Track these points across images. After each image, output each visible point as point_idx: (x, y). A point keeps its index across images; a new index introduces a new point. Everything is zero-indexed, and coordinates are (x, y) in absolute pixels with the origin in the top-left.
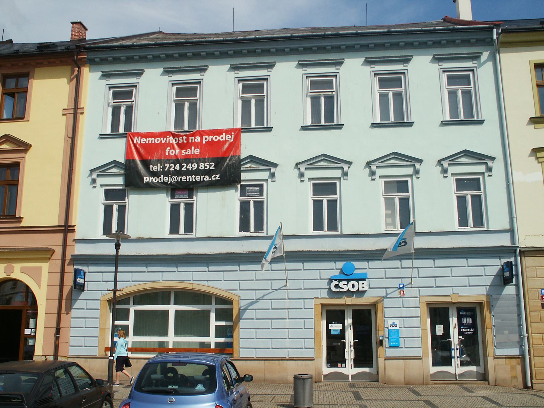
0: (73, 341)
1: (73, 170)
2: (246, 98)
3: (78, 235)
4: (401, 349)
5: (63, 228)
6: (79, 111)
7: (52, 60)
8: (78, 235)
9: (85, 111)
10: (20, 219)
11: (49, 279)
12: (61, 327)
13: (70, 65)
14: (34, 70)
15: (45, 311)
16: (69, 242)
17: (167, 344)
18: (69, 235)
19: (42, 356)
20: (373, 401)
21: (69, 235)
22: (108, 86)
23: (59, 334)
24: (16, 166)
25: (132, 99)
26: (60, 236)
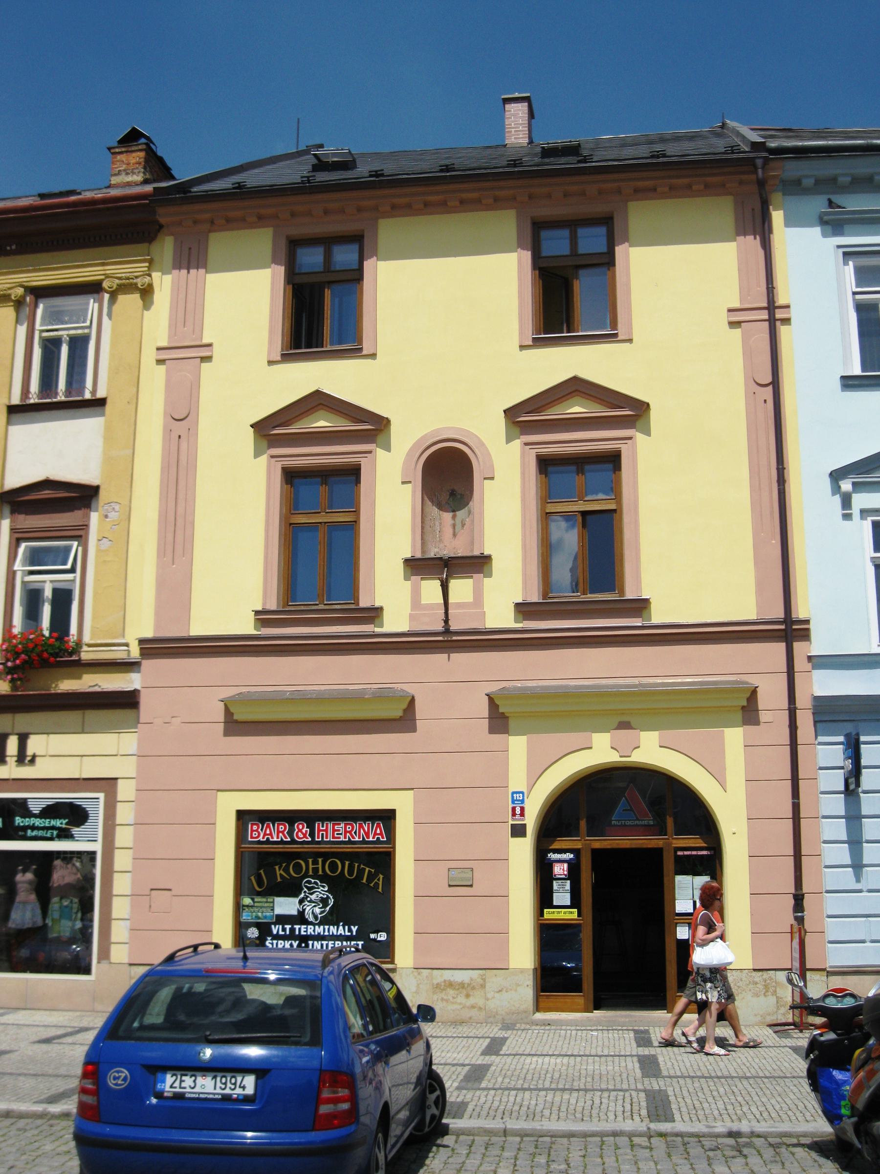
0: (834, 929)
1: (785, 471)
2: (536, 317)
3: (819, 645)
4: (203, 955)
5: (783, 627)
6: (779, 314)
7: (680, 181)
8: (819, 645)
9: (794, 314)
10: (374, 614)
11: (749, 763)
12: (804, 891)
13: (730, 194)
14: (626, 207)
15: (413, 857)
16: (800, 664)
17: (239, 944)
18: (797, 646)
19: (755, 970)
20: (765, 1080)
21: (797, 646)
22: (841, 250)
23: (803, 911)
24: (353, 473)
25: (84, 322)
26: (780, 648)
